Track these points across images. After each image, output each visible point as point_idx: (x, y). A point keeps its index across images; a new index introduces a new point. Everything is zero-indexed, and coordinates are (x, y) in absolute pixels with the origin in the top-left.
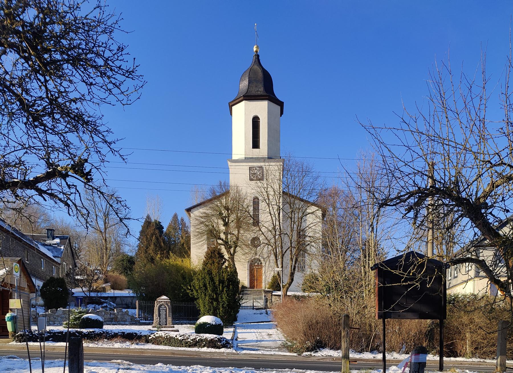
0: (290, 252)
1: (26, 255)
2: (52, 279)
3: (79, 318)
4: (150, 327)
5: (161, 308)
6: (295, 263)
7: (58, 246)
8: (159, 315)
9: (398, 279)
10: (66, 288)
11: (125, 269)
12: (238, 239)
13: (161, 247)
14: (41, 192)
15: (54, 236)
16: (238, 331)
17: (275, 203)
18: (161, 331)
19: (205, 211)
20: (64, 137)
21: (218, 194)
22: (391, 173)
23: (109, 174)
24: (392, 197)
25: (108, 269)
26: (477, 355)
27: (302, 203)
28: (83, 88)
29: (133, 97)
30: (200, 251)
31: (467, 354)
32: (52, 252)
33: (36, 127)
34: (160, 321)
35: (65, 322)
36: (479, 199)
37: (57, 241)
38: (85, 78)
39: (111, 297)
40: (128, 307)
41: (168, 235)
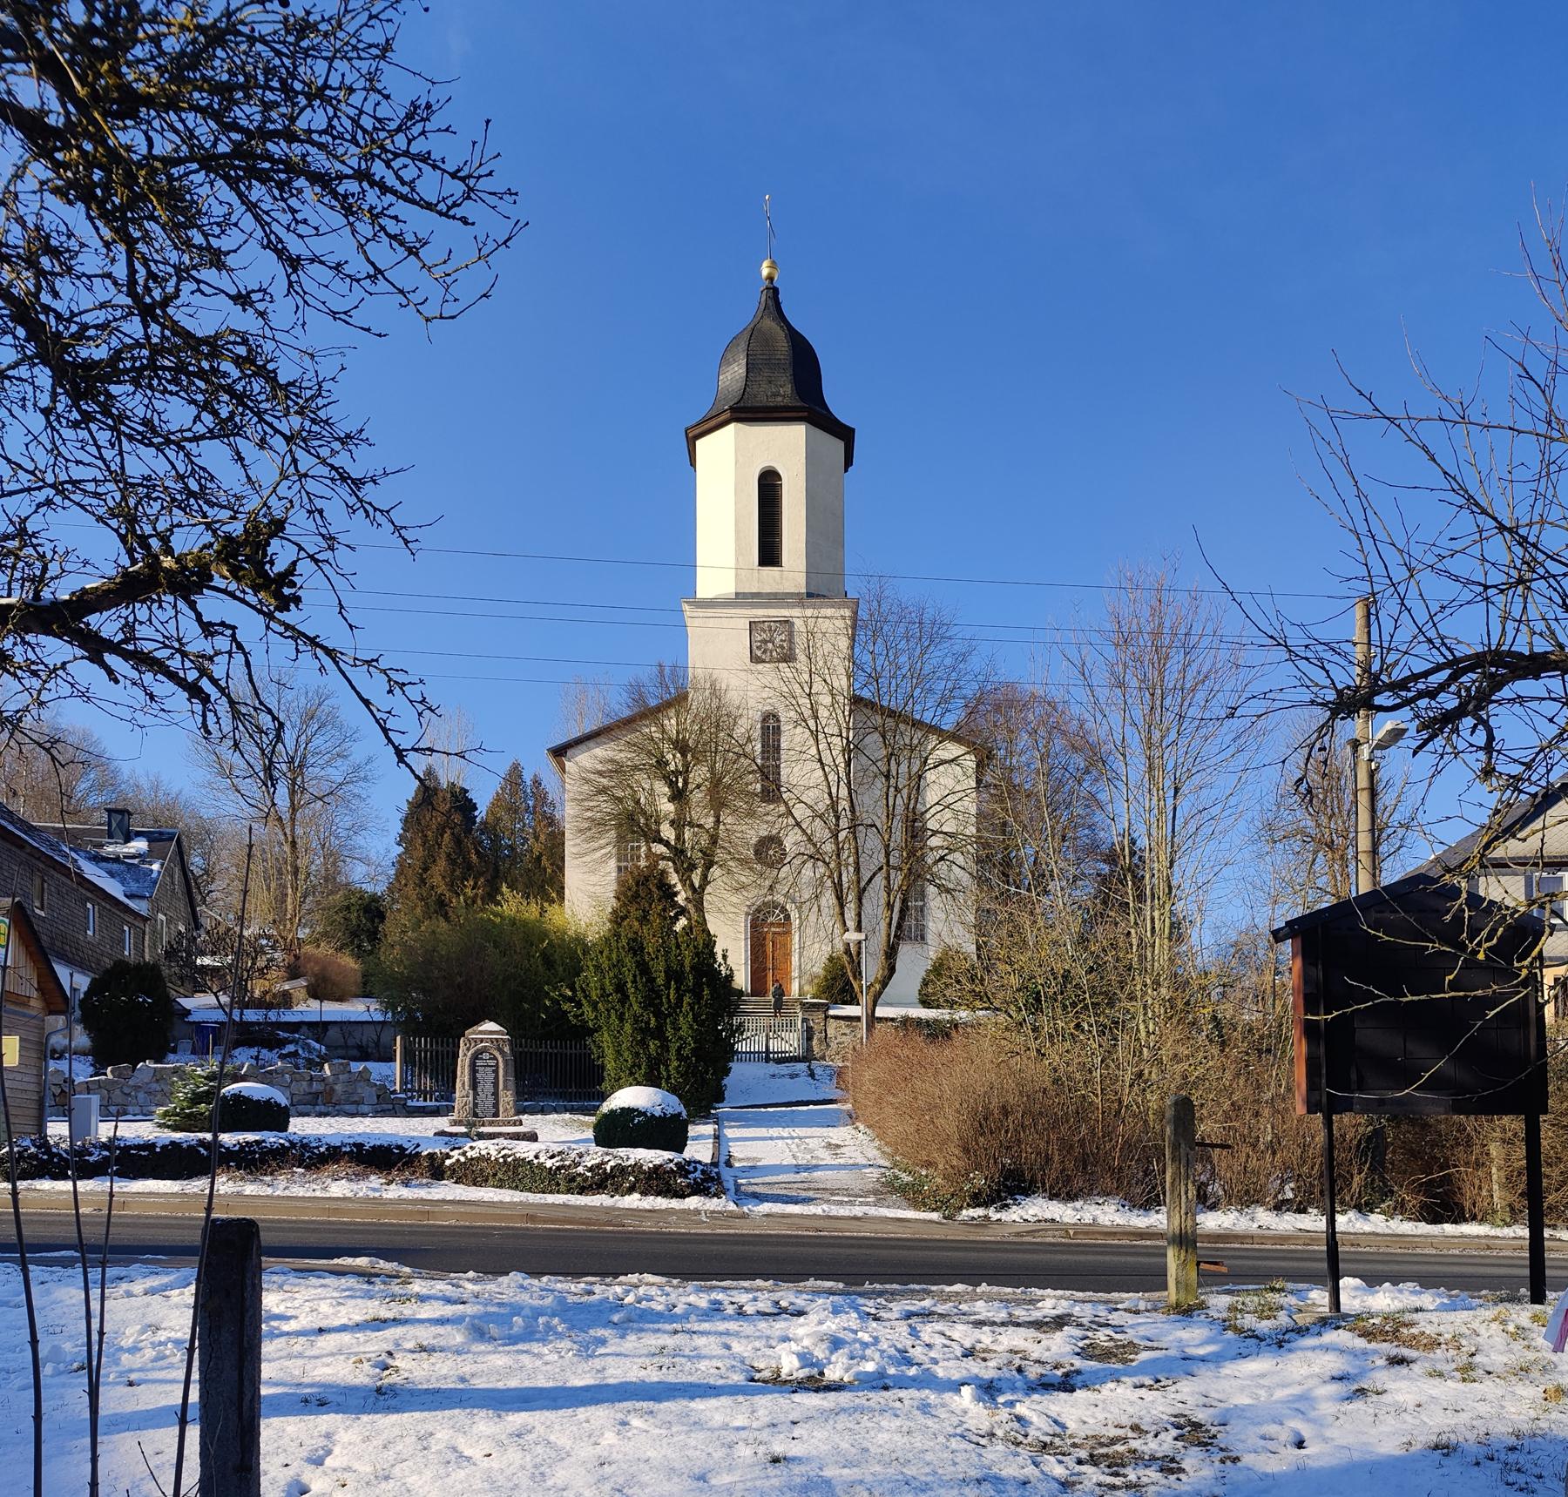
0: (884, 882)
1: (36, 891)
2: (121, 967)
4: (442, 1123)
5: (479, 1062)
7: (143, 862)
8: (474, 1084)
10: (168, 996)
11: (354, 934)
12: (714, 840)
14: (95, 647)
15: (129, 832)
17: (836, 731)
18: (481, 1136)
19: (611, 754)
20: (187, 455)
21: (653, 703)
25: (300, 935)
29: (468, 286)
30: (594, 879)
31: (1495, 1212)
34: (476, 1105)
37: (140, 845)
39: (310, 1024)
41: (489, 828)
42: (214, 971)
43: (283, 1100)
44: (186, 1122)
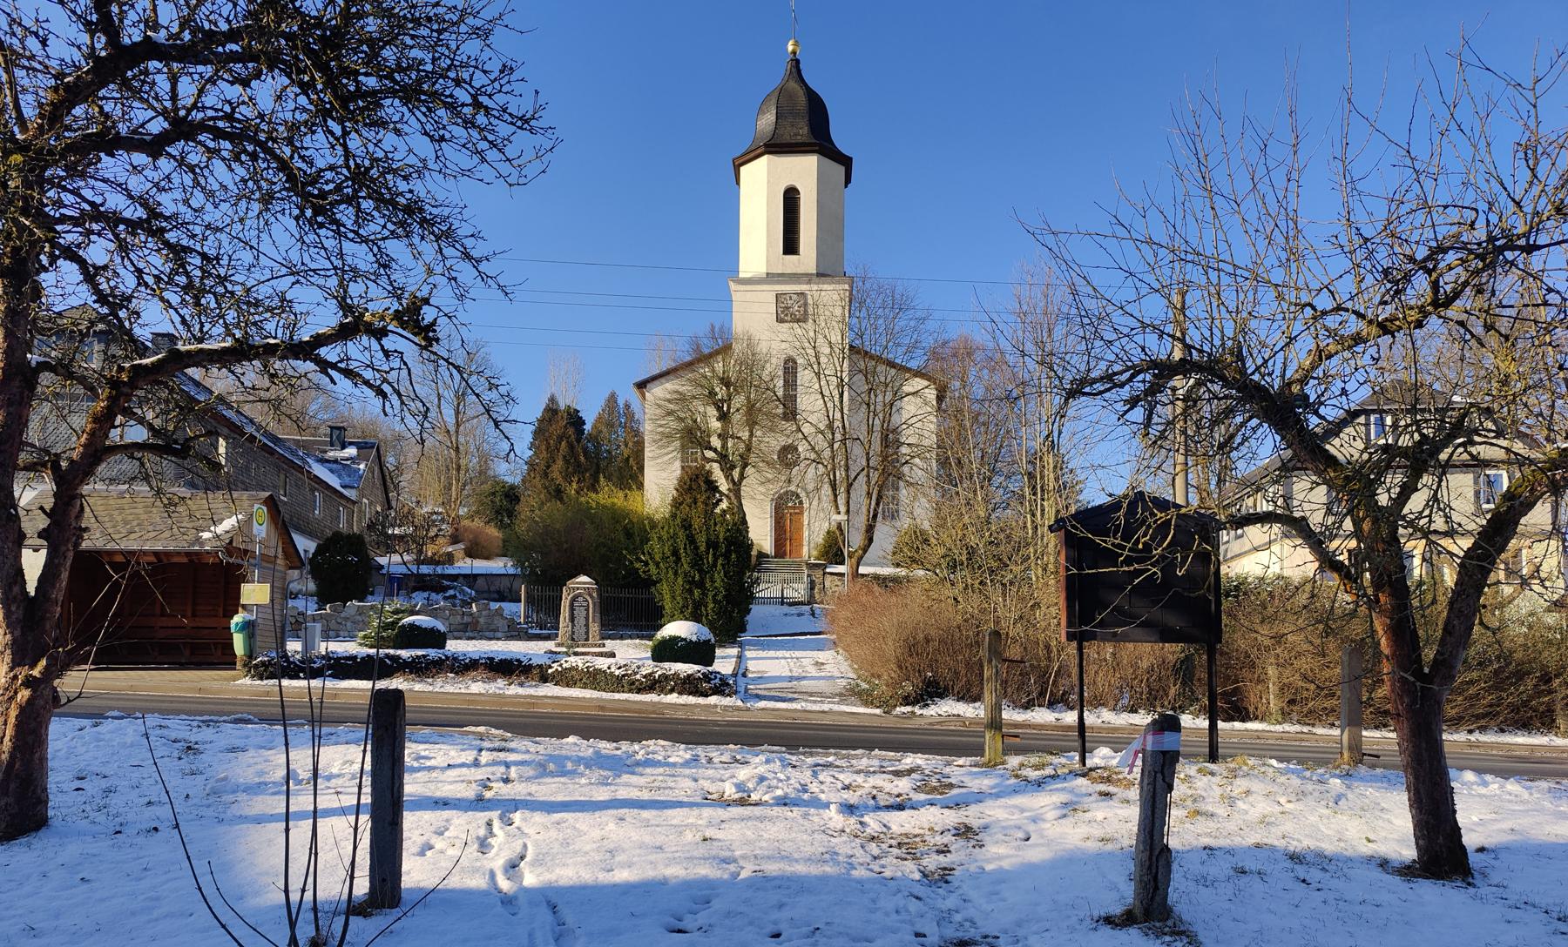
2: (337, 535)
3: (394, 623)
6: (878, 504)
8: (572, 619)
9: (1110, 557)
11: (498, 512)
12: (749, 448)
13: (579, 465)
14: (324, 366)
16: (748, 654)
18: (576, 654)
21: (706, 351)
22: (1092, 326)
23: (474, 321)
24: (1095, 374)
26: (1295, 716)
27: (893, 371)
28: (425, 147)
29: (530, 171)
30: (664, 475)
32: (339, 477)
33: (321, 226)
35: (361, 634)
36: (1289, 385)
37: (351, 451)
38: (428, 127)
39: (465, 576)
40: (502, 599)
41: (594, 438)
42: (401, 538)
43: (442, 628)
44: (379, 643)
